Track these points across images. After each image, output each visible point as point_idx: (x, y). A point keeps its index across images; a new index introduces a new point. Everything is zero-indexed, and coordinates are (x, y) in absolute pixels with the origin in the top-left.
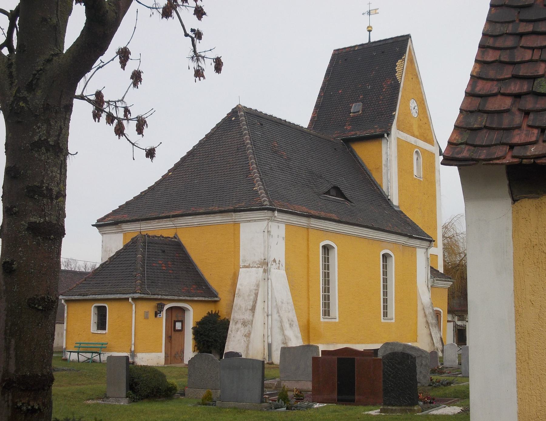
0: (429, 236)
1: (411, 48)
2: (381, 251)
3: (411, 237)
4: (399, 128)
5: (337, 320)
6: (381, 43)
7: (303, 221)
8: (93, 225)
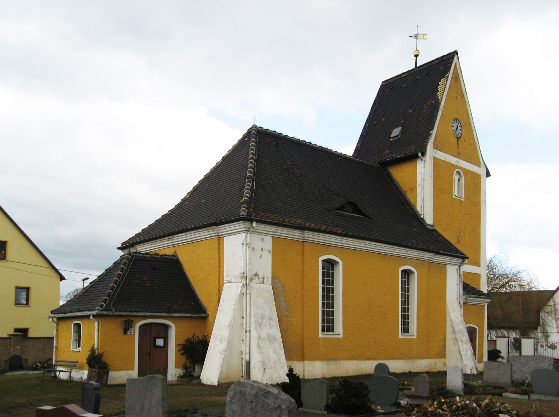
0: (461, 253)
1: (458, 65)
2: (401, 266)
3: (437, 253)
4: (436, 147)
5: (341, 336)
6: (427, 66)
7: (296, 234)
8: (118, 248)
